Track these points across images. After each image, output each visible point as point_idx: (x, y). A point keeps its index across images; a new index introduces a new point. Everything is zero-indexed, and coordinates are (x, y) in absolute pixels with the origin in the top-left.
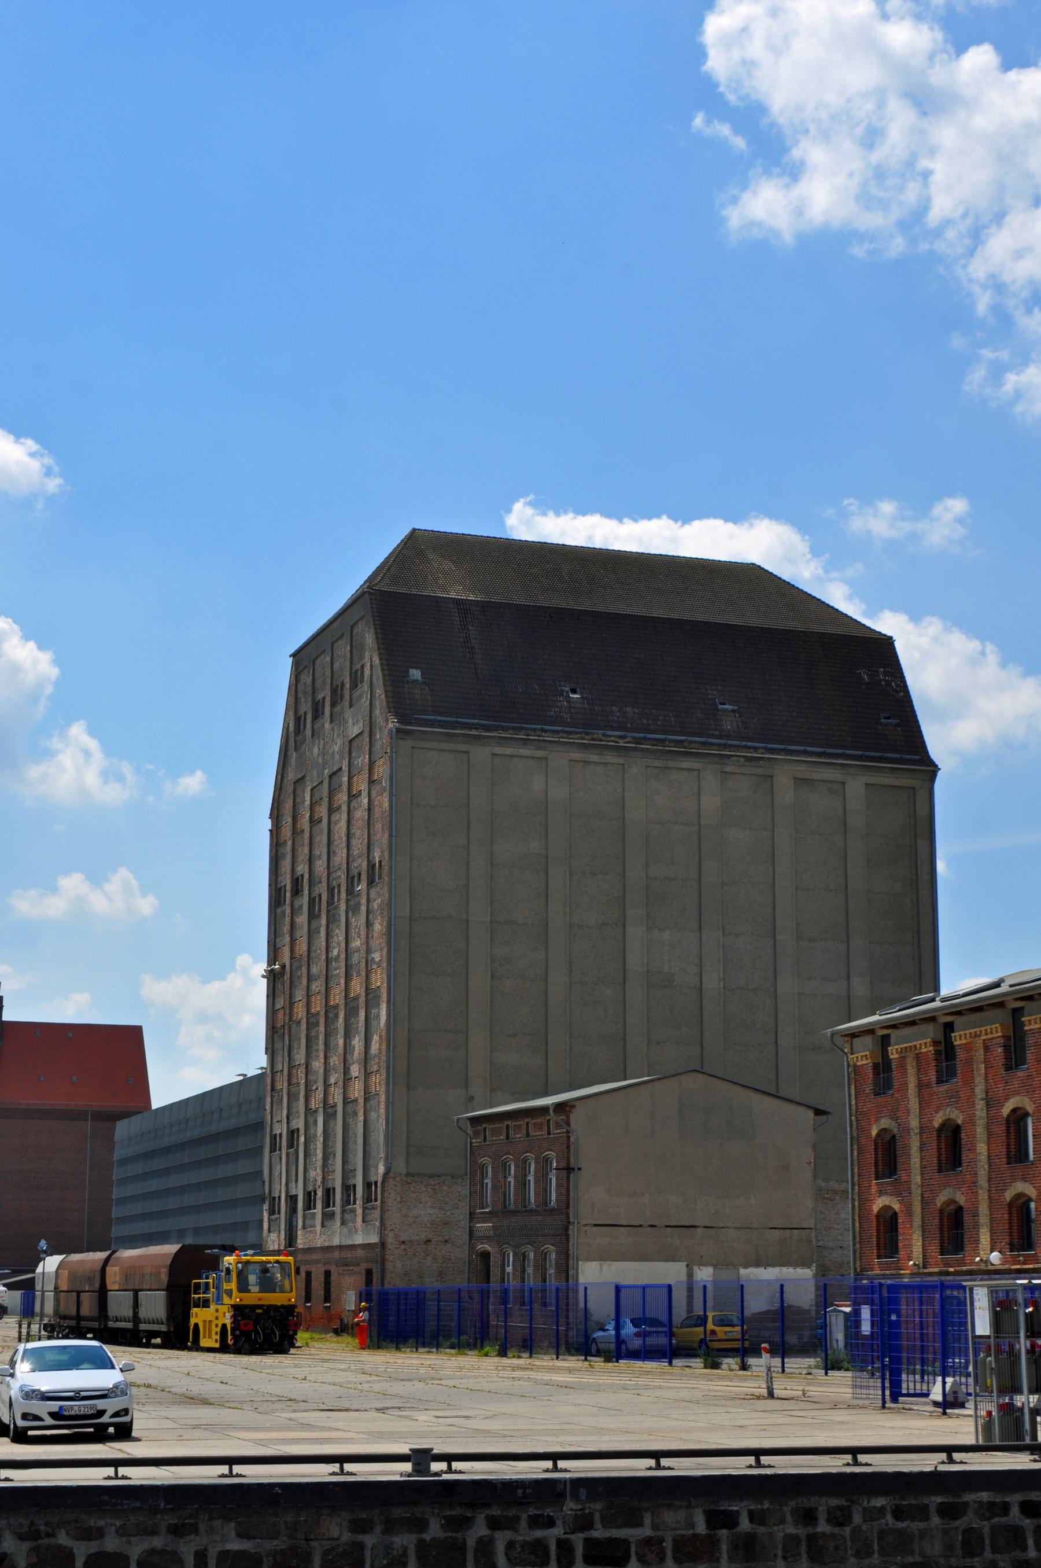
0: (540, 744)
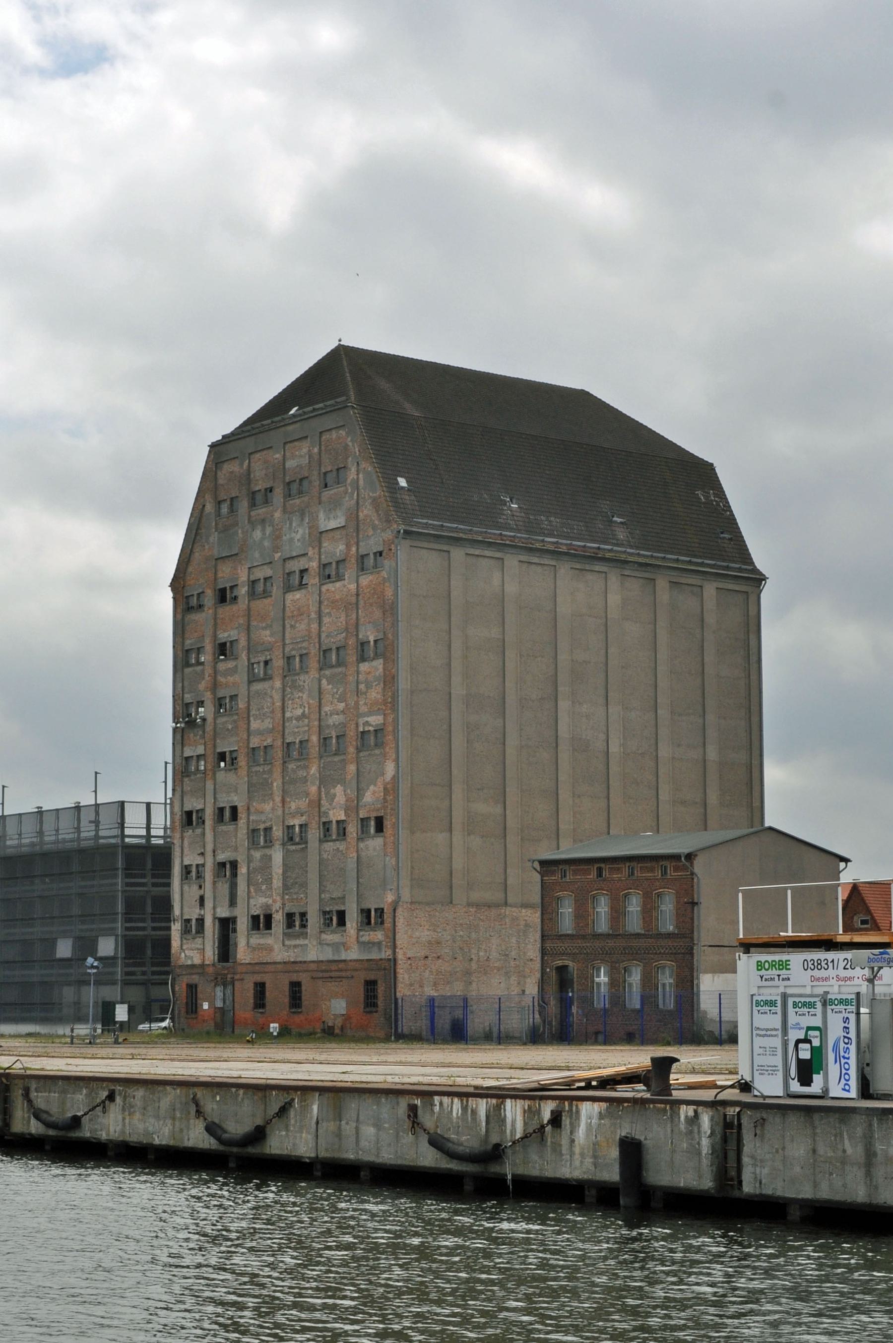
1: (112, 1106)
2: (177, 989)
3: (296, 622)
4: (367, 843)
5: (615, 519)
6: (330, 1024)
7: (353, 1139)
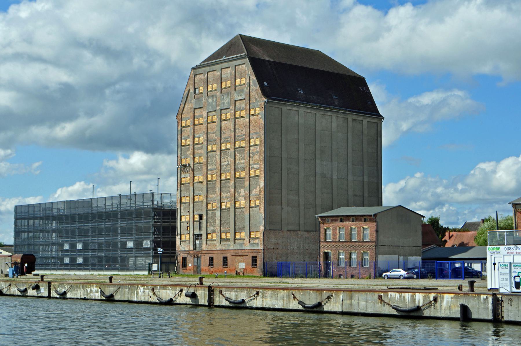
0: (298, 107)
7: (357, 305)
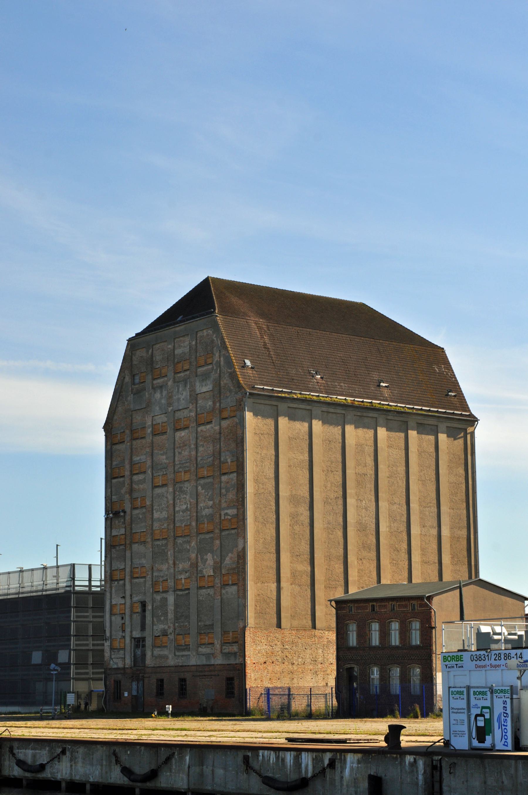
1: (64, 757)
2: (108, 683)
3: (182, 450)
4: (227, 590)
5: (382, 384)
6: (204, 706)
